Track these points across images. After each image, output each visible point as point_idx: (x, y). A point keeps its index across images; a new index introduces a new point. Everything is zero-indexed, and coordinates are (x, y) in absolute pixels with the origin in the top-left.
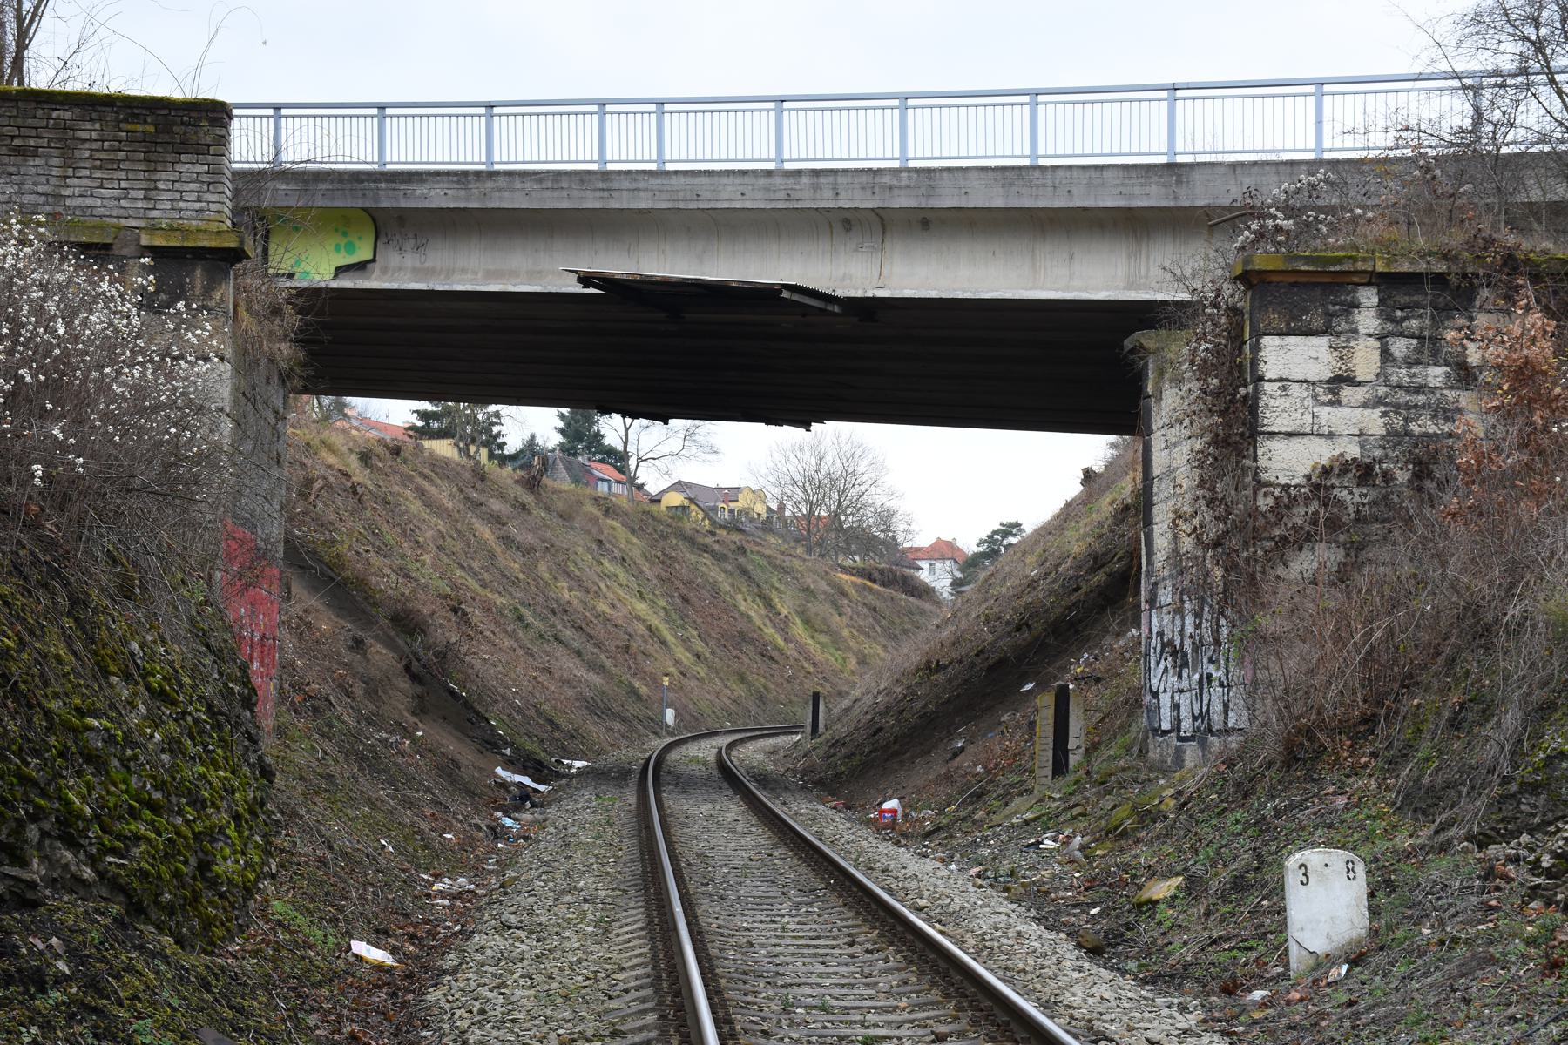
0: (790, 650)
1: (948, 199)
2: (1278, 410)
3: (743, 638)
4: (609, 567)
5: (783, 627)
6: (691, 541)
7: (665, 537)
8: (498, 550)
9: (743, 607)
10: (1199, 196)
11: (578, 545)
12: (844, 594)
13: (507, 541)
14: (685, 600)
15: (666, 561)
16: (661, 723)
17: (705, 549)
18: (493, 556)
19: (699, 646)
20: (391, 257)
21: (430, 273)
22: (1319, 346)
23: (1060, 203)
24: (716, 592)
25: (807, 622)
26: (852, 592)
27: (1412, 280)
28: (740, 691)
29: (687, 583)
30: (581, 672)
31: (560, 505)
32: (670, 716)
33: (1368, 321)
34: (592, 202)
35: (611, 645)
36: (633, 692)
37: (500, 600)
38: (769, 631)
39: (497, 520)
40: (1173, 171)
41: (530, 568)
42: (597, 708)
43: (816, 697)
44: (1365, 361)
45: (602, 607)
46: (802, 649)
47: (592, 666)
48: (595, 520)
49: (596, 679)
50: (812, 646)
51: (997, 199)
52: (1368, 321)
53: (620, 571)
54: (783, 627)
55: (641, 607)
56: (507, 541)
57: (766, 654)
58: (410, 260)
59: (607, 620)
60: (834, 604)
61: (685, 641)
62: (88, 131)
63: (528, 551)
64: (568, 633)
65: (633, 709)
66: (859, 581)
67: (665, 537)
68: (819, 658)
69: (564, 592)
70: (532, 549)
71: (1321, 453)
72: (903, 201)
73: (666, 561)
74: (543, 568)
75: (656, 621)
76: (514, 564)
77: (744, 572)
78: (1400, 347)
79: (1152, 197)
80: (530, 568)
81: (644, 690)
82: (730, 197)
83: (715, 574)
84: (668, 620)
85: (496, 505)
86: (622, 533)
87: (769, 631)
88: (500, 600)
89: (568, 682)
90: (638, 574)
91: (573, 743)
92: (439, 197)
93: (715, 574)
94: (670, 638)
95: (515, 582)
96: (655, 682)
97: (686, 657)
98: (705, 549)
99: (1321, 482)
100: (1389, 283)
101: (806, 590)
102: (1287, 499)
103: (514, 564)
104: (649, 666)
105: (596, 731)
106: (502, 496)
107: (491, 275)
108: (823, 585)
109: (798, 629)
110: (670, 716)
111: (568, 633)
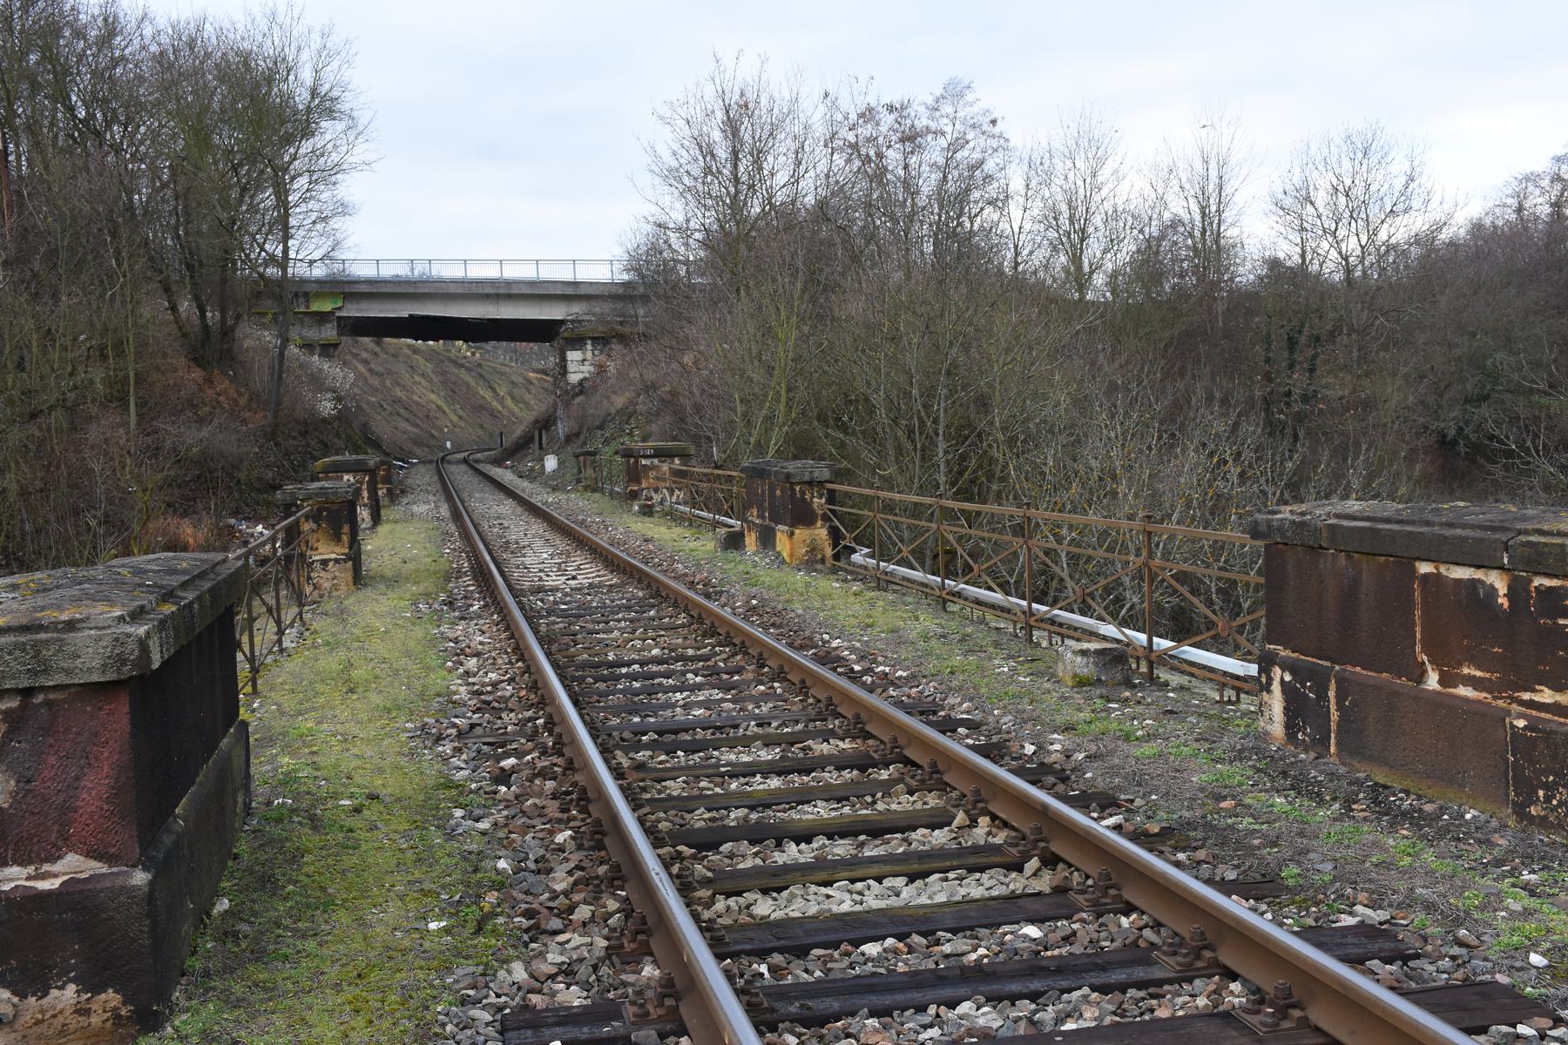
0: (505, 412)
1: (515, 291)
2: (571, 367)
3: (482, 408)
4: (417, 378)
5: (501, 401)
6: (455, 363)
7: (442, 362)
8: (368, 376)
9: (482, 393)
10: (582, 291)
11: (401, 368)
12: (532, 383)
13: (371, 371)
14: (453, 391)
15: (444, 373)
16: (445, 447)
17: (462, 366)
18: (366, 379)
19: (461, 413)
20: (349, 306)
21: (362, 310)
22: (579, 352)
23: (546, 292)
24: (468, 385)
25: (513, 398)
26: (536, 382)
27: (597, 338)
28: (481, 432)
29: (454, 383)
30: (409, 428)
31: (392, 351)
32: (448, 444)
33: (589, 347)
34: (411, 290)
35: (420, 415)
36: (432, 435)
37: (373, 399)
38: (495, 404)
39: (366, 362)
40: (575, 284)
41: (383, 383)
42: (418, 442)
43: (501, 434)
44: (589, 355)
45: (416, 398)
46: (510, 411)
47: (413, 425)
48: (408, 356)
49: (414, 430)
50: (516, 410)
51: (528, 291)
52: (589, 347)
53: (422, 381)
54: (501, 401)
55: (433, 397)
56: (371, 371)
57: (493, 414)
58: (355, 306)
59: (417, 404)
60: (527, 389)
61: (454, 411)
62: (306, 319)
63: (380, 375)
64: (402, 411)
65: (432, 442)
66: (539, 376)
67: (442, 362)
68: (520, 415)
69: (399, 393)
70: (382, 374)
71: (581, 376)
72: (502, 291)
73: (444, 373)
74: (388, 383)
75: (440, 403)
76: (375, 382)
77: (482, 376)
78: (596, 352)
79: (569, 291)
80: (383, 383)
81: (436, 434)
82: (452, 289)
83: (467, 378)
84: (446, 401)
85: (365, 355)
86: (422, 362)
87: (495, 404)
88: (373, 399)
89: (404, 432)
90: (431, 381)
91: (412, 454)
92: (364, 289)
93: (467, 378)
94: (447, 410)
95: (377, 390)
96: (441, 430)
97: (455, 418)
98: (462, 366)
99: (581, 383)
100: (595, 340)
101: (513, 382)
102: (574, 387)
103: (375, 382)
104: (438, 423)
105: (418, 451)
106: (366, 350)
107: (380, 311)
108: (521, 380)
109: (509, 402)
110: (448, 444)
111: (402, 411)
